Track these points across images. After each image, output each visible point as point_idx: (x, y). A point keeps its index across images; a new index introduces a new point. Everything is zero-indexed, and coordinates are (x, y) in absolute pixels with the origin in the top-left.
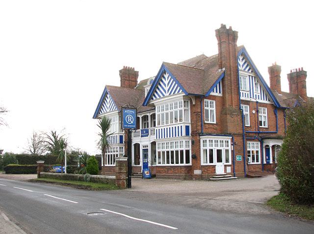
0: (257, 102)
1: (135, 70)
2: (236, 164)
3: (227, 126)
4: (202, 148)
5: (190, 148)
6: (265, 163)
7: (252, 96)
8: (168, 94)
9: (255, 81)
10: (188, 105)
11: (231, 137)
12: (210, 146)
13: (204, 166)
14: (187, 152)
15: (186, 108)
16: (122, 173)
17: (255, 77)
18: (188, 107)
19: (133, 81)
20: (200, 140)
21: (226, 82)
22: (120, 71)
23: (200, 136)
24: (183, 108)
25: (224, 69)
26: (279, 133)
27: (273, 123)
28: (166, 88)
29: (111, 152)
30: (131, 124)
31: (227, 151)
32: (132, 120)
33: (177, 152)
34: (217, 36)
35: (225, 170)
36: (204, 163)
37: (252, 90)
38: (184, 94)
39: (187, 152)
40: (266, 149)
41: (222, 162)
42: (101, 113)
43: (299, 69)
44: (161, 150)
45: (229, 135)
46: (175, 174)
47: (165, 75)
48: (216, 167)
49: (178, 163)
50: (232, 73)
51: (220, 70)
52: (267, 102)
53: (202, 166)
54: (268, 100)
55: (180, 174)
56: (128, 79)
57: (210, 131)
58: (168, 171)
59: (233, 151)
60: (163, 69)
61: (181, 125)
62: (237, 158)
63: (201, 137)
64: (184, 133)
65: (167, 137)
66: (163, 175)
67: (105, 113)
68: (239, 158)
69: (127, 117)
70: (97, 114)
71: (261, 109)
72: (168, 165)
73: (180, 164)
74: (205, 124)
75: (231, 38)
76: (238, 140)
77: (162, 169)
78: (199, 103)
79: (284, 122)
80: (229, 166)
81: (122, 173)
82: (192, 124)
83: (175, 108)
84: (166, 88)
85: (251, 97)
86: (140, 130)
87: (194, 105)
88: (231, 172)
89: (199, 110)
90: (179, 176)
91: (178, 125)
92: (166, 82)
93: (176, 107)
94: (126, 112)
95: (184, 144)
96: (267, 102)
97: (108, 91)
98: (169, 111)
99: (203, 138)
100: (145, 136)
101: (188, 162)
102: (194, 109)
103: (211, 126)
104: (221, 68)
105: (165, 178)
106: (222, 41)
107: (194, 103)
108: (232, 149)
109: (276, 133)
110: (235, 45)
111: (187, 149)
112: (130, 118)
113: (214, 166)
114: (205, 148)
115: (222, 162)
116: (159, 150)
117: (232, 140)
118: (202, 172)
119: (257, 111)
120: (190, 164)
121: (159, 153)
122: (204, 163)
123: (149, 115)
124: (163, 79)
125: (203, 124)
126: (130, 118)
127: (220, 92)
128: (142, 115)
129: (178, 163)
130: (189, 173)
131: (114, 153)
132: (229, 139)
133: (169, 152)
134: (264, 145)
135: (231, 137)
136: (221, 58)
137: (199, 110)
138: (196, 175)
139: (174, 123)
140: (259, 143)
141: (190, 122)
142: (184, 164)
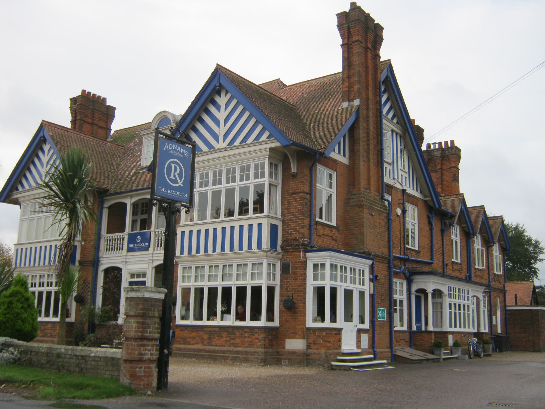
0: (404, 191)
1: (108, 104)
2: (377, 328)
3: (362, 234)
4: (311, 284)
5: (277, 282)
6: (414, 328)
7: (396, 177)
8: (223, 144)
9: (401, 145)
10: (276, 174)
11: (370, 262)
12: (332, 280)
13: (315, 330)
14: (271, 290)
15: (273, 180)
16: (148, 339)
17: (400, 137)
18: (276, 178)
19: (101, 127)
20: (305, 262)
21: (361, 133)
22: (74, 101)
23: (306, 251)
24: (266, 181)
25: (357, 102)
26: (434, 266)
27: (427, 241)
28: (221, 131)
29: (41, 285)
30: (178, 189)
31: (362, 294)
32: (180, 175)
33: (241, 290)
34: (340, 26)
35: (359, 342)
36: (315, 320)
37: (395, 164)
38: (276, 144)
39: (271, 290)
40: (418, 299)
41: (352, 321)
42: (27, 187)
43: (446, 143)
44: (192, 284)
45: (366, 255)
46: (231, 349)
47: (217, 99)
48: (343, 332)
49: (201, 319)
50: (371, 114)
51: (345, 105)
52: (417, 194)
53: (309, 329)
54: (419, 191)
55: (249, 349)
56: (90, 121)
57: (327, 241)
58: (209, 338)
59: (372, 296)
60: (216, 82)
61: (260, 221)
62: (379, 314)
63: (308, 255)
64: (266, 243)
65: (214, 250)
66: (194, 350)
67: (32, 189)
68: (381, 314)
69: (169, 167)
70: (11, 191)
71: (409, 207)
72: (239, 323)
73: (248, 323)
74: (317, 223)
75: (371, 37)
76: (382, 270)
77: (194, 334)
78: (307, 172)
79: (441, 242)
80: (364, 331)
81: (148, 339)
82: (283, 222)
83: (214, 184)
84: (221, 131)
85: (394, 179)
86: (125, 235)
87: (294, 176)
88: (369, 348)
89: (307, 189)
90: (246, 353)
91: (224, 225)
92: (221, 116)
93: (245, 177)
94: (166, 147)
95: (265, 269)
96: (417, 194)
97: (47, 134)
98: (223, 187)
99: (312, 258)
100: (140, 249)
101: (270, 318)
102: (293, 185)
103: (327, 231)
104: (350, 100)
105: (202, 357)
106: (355, 38)
107: (294, 170)
108: (372, 292)
109: (429, 264)
110: (377, 56)
111: (271, 283)
112: (176, 170)
113: (339, 331)
114: (319, 283)
115: (352, 321)
116: (186, 284)
117: (372, 267)
118: (309, 347)
119: (404, 211)
120: (276, 323)
121: (186, 292)
122: (315, 320)
123: (129, 202)
124: (212, 109)
125: (313, 225)
126: (176, 170)
127: (344, 155)
128: (134, 200)
129: (201, 319)
130: (271, 345)
131: (41, 289)
132: (364, 264)
133: (189, 289)
134: (414, 288)
135: (370, 262)
136: (349, 77)
137: (307, 189)
138: (293, 353)
139: (209, 219)
140: (405, 283)
141: (279, 215)
142: (263, 322)
